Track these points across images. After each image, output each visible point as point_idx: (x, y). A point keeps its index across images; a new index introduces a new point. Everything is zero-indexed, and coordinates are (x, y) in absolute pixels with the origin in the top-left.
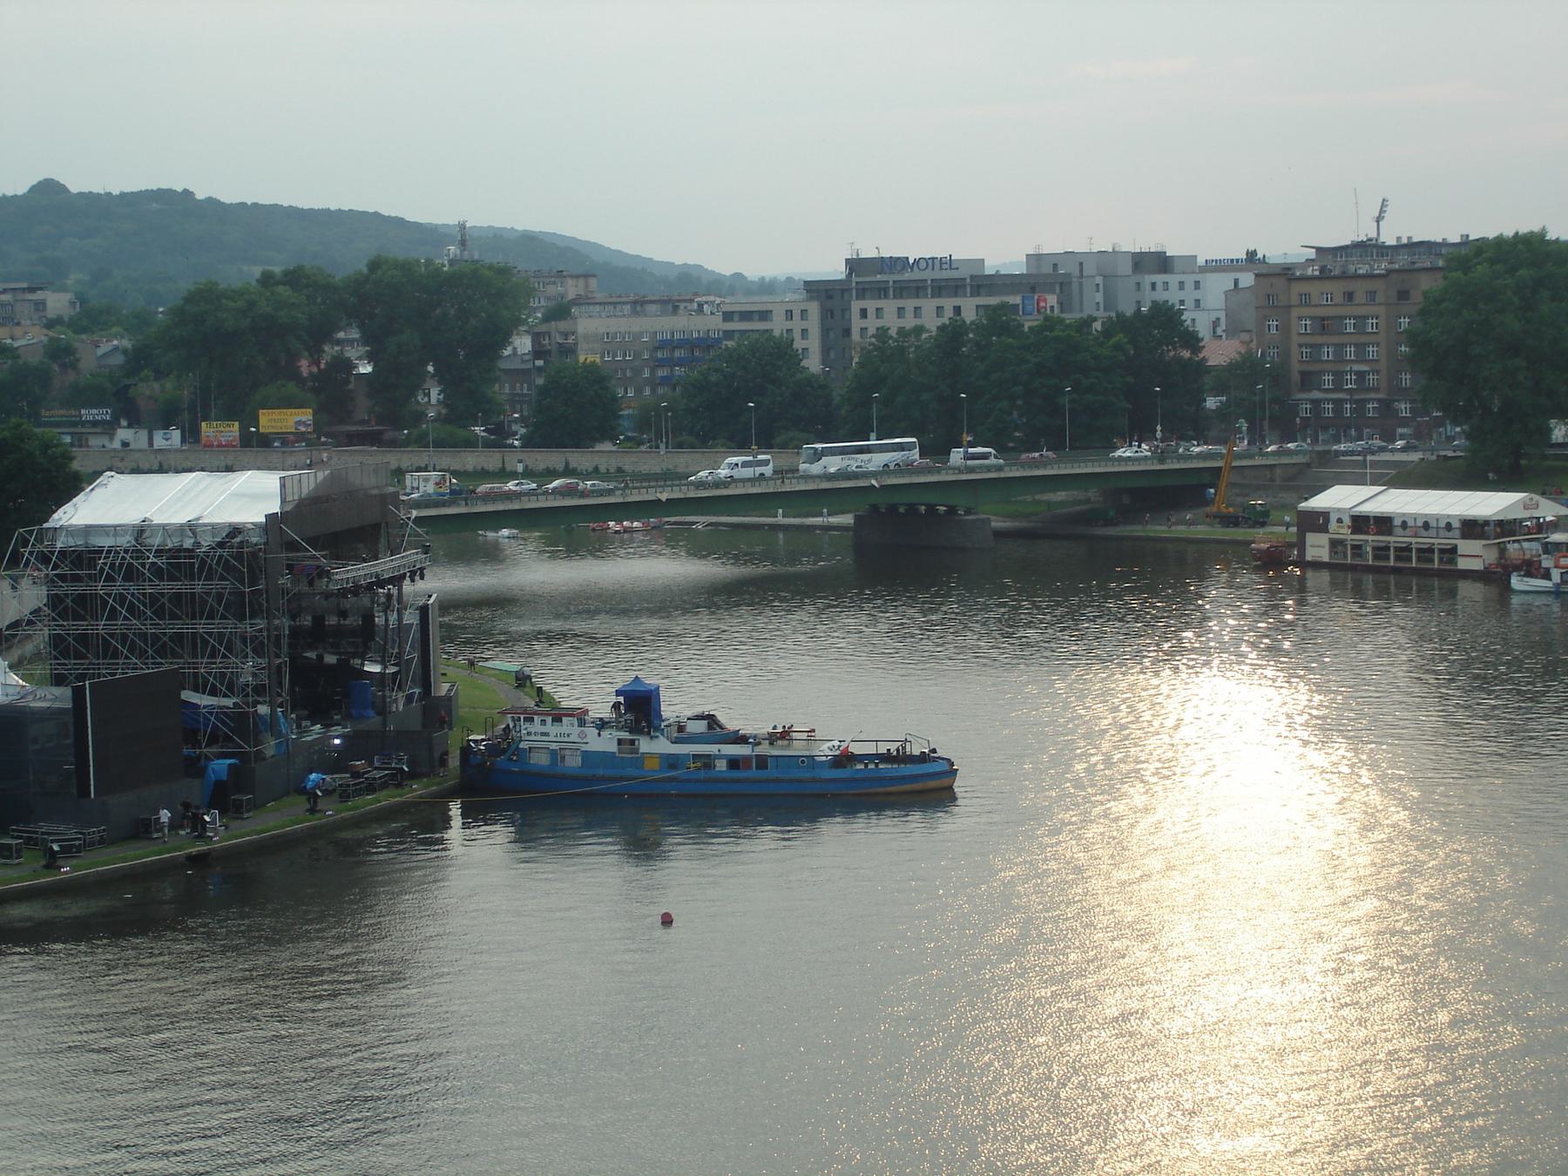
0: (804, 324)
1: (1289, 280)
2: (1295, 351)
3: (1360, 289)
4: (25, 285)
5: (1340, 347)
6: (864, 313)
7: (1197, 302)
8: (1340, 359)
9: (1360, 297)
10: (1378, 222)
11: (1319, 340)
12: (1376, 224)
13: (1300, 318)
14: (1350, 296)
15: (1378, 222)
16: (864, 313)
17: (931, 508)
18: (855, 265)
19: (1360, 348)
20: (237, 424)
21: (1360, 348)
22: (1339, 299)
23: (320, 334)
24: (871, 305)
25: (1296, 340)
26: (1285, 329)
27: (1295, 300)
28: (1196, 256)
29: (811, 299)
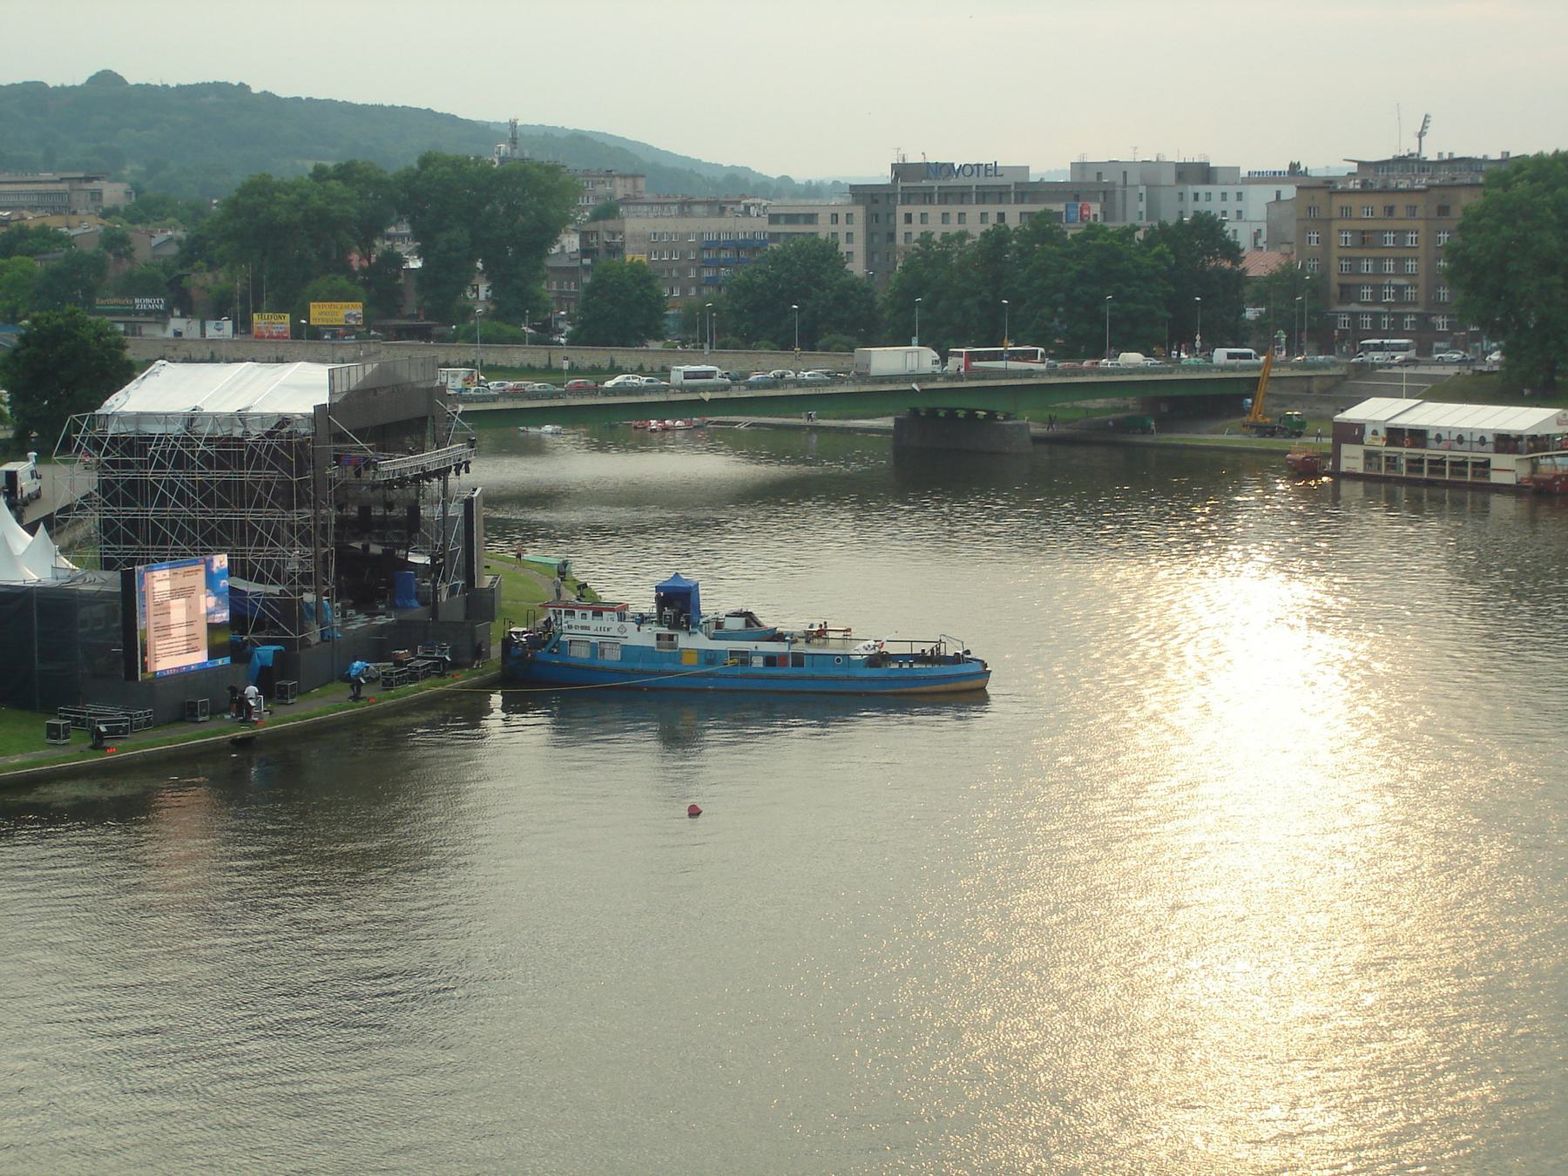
0: (849, 228)
1: (1331, 193)
2: (1334, 263)
3: (1400, 203)
4: (81, 175)
5: (1379, 261)
6: (908, 218)
7: (1239, 212)
8: (1379, 273)
9: (1400, 212)
10: (1420, 137)
11: (1358, 253)
12: (1417, 139)
13: (1341, 231)
14: (1390, 210)
15: (1420, 137)
16: (908, 218)
17: (971, 414)
18: (900, 170)
19: (1400, 262)
20: (288, 316)
21: (1400, 262)
22: (1379, 212)
23: (371, 228)
24: (916, 210)
25: (1336, 253)
26: (1325, 242)
27: (1336, 213)
28: (1028, 167)
29: (857, 203)
